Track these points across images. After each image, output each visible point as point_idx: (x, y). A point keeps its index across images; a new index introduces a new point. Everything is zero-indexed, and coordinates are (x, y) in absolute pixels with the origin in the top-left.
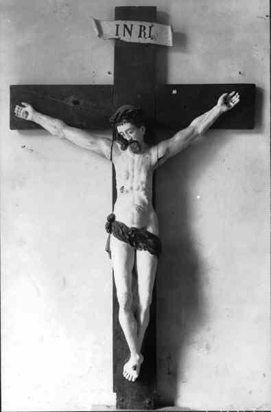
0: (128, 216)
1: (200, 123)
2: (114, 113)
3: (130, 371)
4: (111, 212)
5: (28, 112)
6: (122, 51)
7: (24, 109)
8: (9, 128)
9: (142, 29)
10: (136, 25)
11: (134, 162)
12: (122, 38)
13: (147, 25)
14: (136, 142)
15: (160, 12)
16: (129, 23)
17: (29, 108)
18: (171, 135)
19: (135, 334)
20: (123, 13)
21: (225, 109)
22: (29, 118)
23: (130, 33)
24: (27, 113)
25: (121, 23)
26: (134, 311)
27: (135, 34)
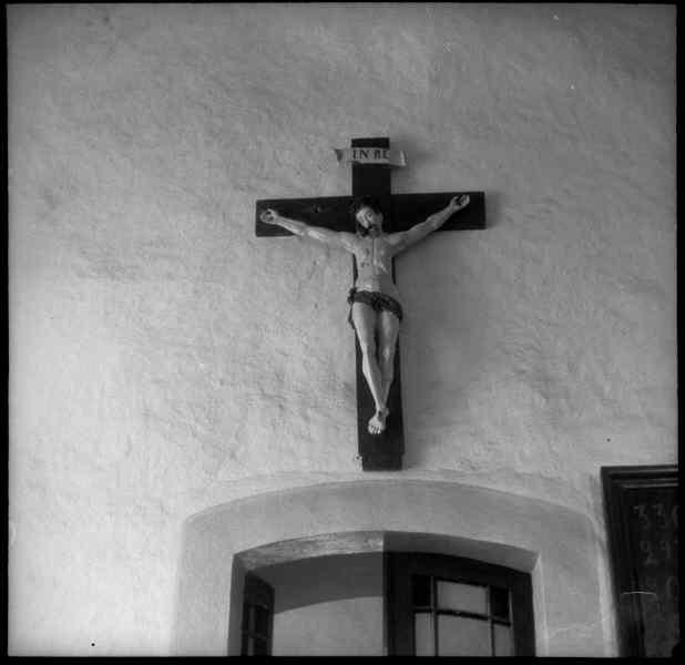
0: (367, 286)
1: (435, 220)
2: (390, 481)
3: (376, 425)
4: (352, 286)
5: (275, 218)
6: (360, 172)
7: (269, 216)
8: (254, 234)
9: (377, 153)
10: (372, 151)
11: (209, 329)
12: (358, 159)
13: (381, 150)
14: (374, 225)
15: (229, 651)
16: (365, 149)
17: (274, 214)
18: (407, 228)
19: (379, 383)
20: (357, 143)
21: (457, 208)
22: (273, 223)
23: (366, 156)
24: (272, 218)
25: (358, 149)
26: (377, 356)
27: (370, 157)
